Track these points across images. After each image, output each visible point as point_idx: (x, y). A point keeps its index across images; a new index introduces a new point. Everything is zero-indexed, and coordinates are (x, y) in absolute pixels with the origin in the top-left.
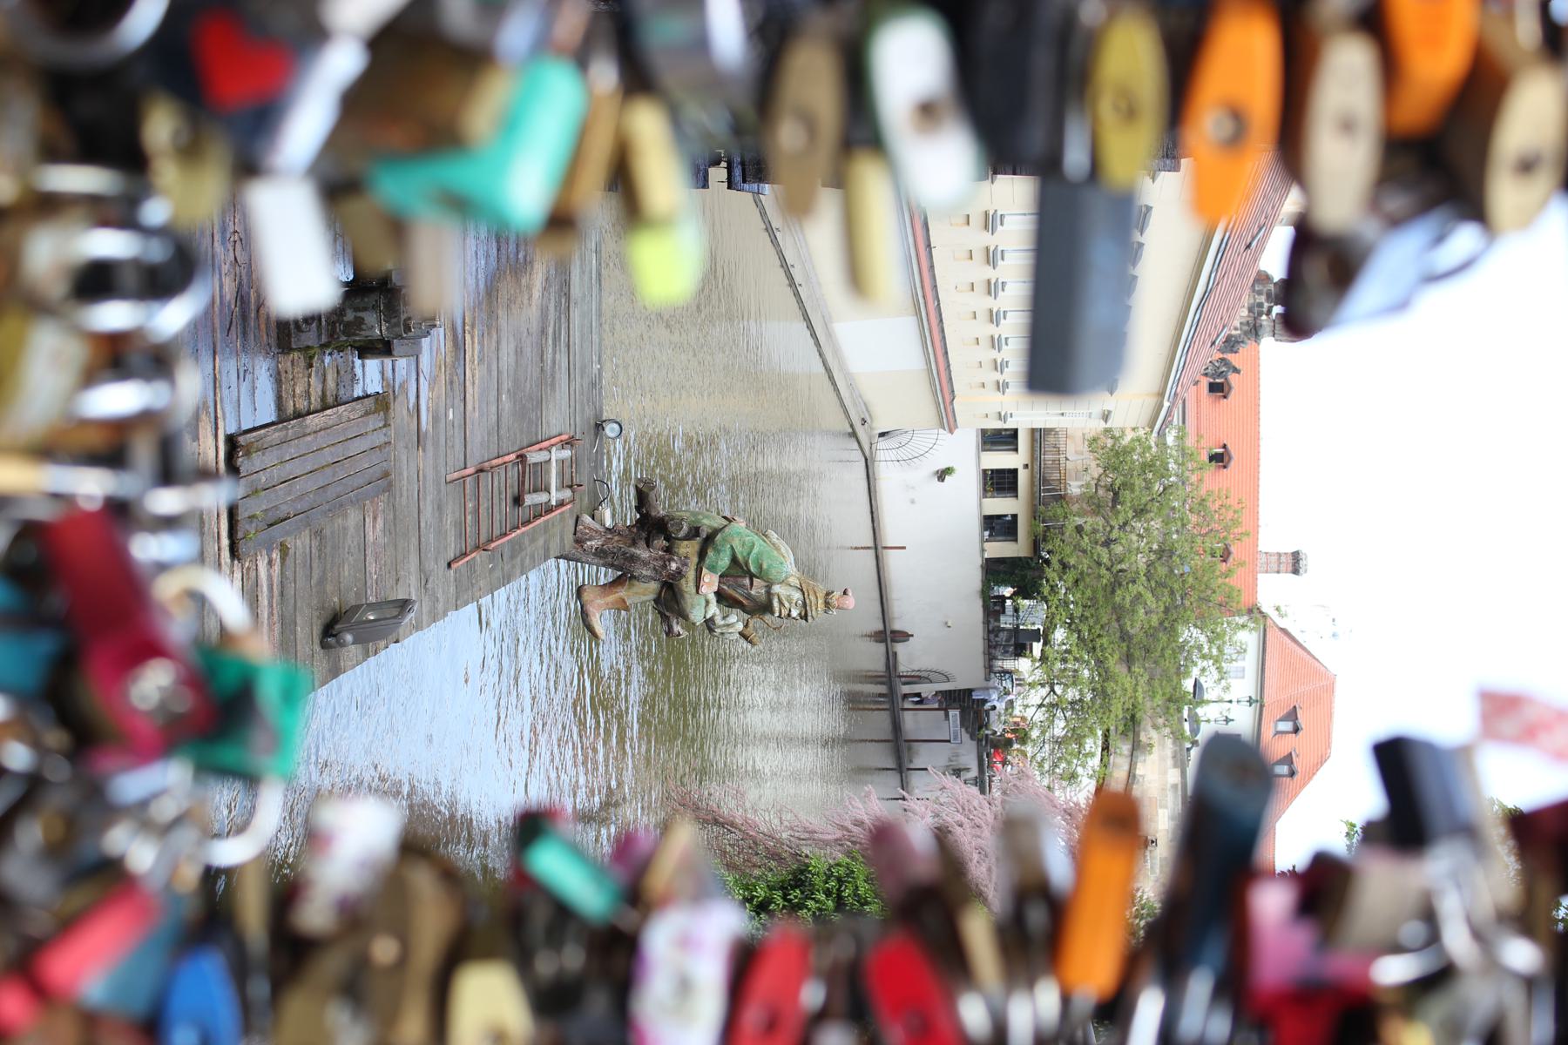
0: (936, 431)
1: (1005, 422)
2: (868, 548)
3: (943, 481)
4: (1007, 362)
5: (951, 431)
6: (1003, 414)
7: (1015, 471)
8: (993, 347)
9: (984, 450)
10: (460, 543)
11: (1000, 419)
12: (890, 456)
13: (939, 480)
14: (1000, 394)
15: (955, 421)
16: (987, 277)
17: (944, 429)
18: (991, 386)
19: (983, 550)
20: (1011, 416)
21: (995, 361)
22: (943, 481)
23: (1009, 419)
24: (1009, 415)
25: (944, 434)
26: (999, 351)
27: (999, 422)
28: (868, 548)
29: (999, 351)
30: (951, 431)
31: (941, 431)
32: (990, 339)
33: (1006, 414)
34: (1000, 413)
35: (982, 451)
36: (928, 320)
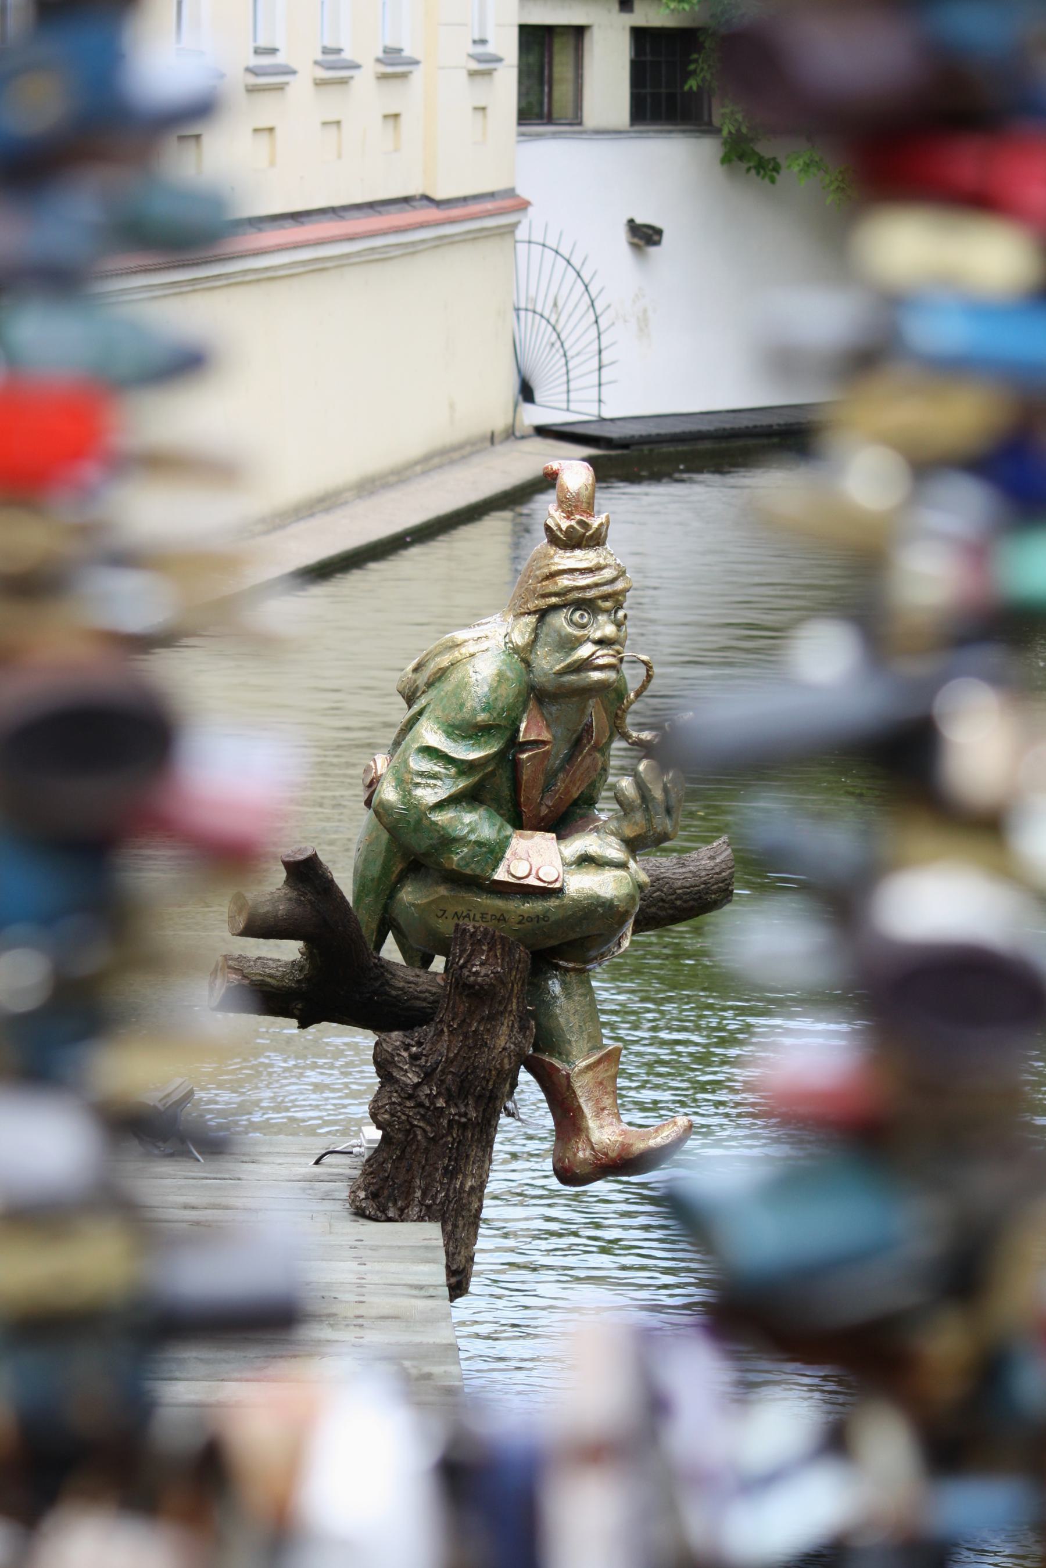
0: (522, 248)
1: (499, 60)
2: (592, 401)
3: (659, 232)
4: (326, 51)
5: (523, 206)
6: (474, 66)
7: (640, 35)
8: (344, 82)
9: (576, 119)
10: (316, 1149)
11: (488, 73)
12: (561, 376)
13: (657, 243)
14: (418, 75)
15: (492, 195)
16: (372, 82)
17: (515, 226)
18: (393, 99)
19: (601, 133)
20: (483, 42)
21: (319, 83)
22: (659, 232)
23: (491, 49)
24: (480, 49)
25: (529, 225)
26: (294, 72)
27: (497, 75)
28: (592, 401)
29: (294, 72)
30: (523, 206)
31: (521, 233)
32: (478, 79)
33: (471, 56)
34: (473, 74)
35: (580, 124)
36: (208, 277)
